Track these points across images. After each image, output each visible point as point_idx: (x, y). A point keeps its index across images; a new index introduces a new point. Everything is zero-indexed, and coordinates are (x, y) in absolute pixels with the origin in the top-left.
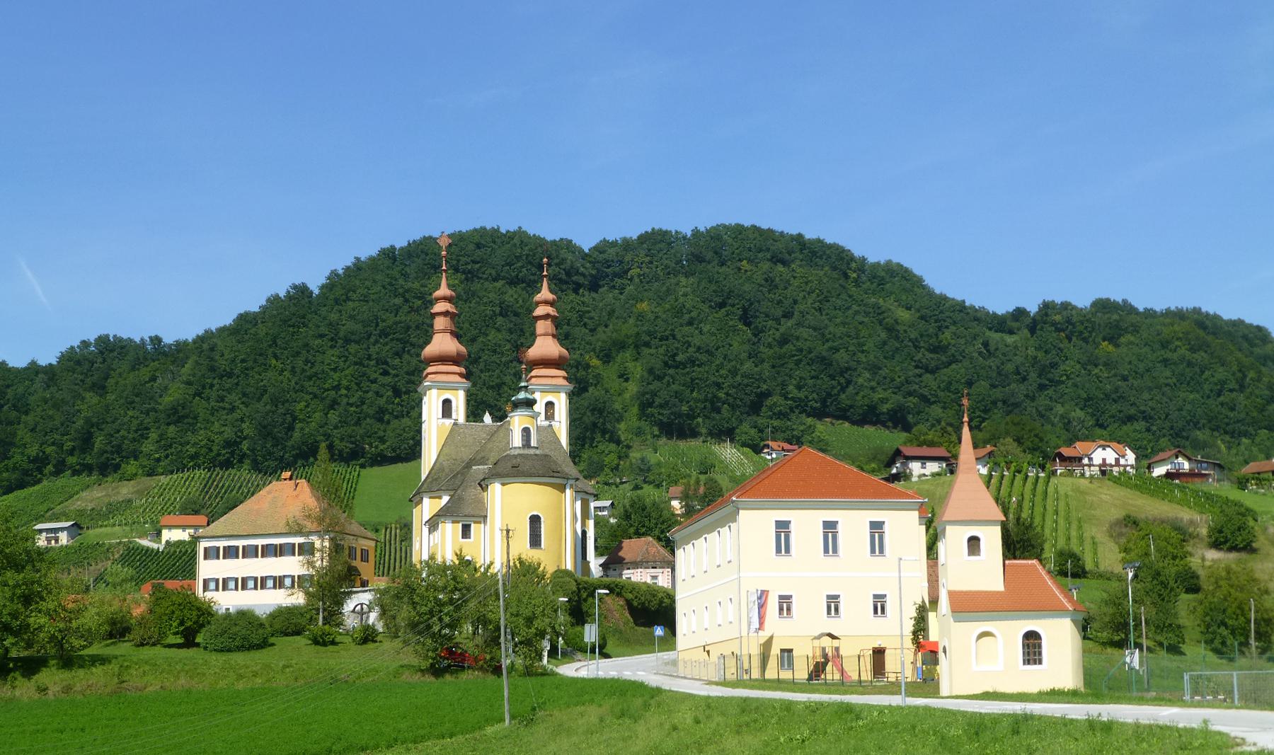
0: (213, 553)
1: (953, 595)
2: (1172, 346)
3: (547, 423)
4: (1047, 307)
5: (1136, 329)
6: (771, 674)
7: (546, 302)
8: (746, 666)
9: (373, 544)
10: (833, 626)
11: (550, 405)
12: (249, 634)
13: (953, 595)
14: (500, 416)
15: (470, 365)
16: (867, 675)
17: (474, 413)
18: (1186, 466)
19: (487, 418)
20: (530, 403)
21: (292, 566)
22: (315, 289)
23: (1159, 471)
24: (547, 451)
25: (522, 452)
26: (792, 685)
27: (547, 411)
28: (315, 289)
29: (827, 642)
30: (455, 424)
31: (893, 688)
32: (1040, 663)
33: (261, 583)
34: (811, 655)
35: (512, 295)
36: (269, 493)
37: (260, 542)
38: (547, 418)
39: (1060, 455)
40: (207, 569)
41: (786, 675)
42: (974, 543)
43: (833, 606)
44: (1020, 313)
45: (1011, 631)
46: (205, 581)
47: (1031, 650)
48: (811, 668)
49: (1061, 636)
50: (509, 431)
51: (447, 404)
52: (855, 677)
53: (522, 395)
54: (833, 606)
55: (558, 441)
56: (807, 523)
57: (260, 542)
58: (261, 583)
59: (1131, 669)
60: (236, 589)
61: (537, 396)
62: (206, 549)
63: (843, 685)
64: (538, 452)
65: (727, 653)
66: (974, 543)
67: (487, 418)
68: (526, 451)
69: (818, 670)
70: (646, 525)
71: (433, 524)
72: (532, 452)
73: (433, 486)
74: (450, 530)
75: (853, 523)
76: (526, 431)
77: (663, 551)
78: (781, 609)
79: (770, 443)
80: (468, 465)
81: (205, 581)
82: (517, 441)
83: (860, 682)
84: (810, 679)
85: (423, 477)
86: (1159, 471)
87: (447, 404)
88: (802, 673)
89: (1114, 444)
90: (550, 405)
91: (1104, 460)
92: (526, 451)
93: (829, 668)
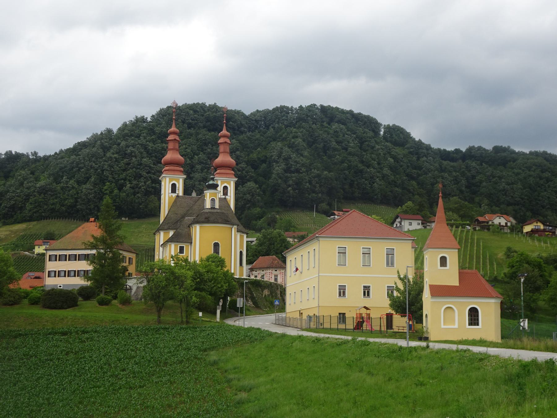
0: (53, 258)
1: (432, 287)
2: (533, 169)
3: (224, 197)
4: (470, 149)
5: (514, 160)
6: (334, 326)
7: (224, 136)
8: (321, 321)
9: (135, 255)
10: (367, 302)
11: (225, 188)
12: (61, 299)
13: (432, 287)
14: (200, 193)
15: (189, 171)
16: (384, 328)
17: (187, 191)
18: (542, 227)
19: (194, 194)
20: (215, 187)
21: (84, 266)
22: (115, 130)
23: (527, 229)
24: (223, 211)
25: (210, 211)
26: (345, 331)
27: (224, 190)
28: (115, 130)
29: (364, 311)
30: (178, 196)
31: (396, 335)
32: (478, 325)
33: (68, 274)
34: (355, 317)
35: (210, 135)
36: (83, 228)
37: (68, 253)
38: (224, 194)
39: (477, 220)
40: (51, 266)
41: (342, 326)
42: (443, 261)
43: (367, 292)
44: (457, 151)
45: (461, 306)
46: (49, 272)
47: (473, 318)
48: (355, 324)
49: (490, 309)
50: (204, 201)
51: (174, 186)
52: (378, 329)
53: (211, 182)
54: (367, 292)
55: (229, 206)
56: (355, 248)
57: (68, 253)
58: (68, 274)
59: (524, 328)
60: (55, 276)
61: (219, 183)
62: (50, 255)
63: (372, 333)
64: (219, 211)
65: (311, 314)
66: (443, 261)
67: (194, 194)
68: (213, 211)
69: (359, 325)
70: (272, 250)
71: (164, 245)
72: (215, 211)
73: (165, 227)
74: (173, 249)
75: (379, 248)
76: (213, 200)
77: (280, 262)
78: (364, 292)
79: (336, 212)
80: (183, 217)
81: (49, 272)
82: (208, 205)
83: (381, 331)
84: (354, 329)
85: (161, 222)
86: (527, 229)
87: (174, 186)
88: (350, 325)
89: (505, 216)
90: (225, 188)
91: (500, 223)
92: (213, 211)
93: (365, 324)
